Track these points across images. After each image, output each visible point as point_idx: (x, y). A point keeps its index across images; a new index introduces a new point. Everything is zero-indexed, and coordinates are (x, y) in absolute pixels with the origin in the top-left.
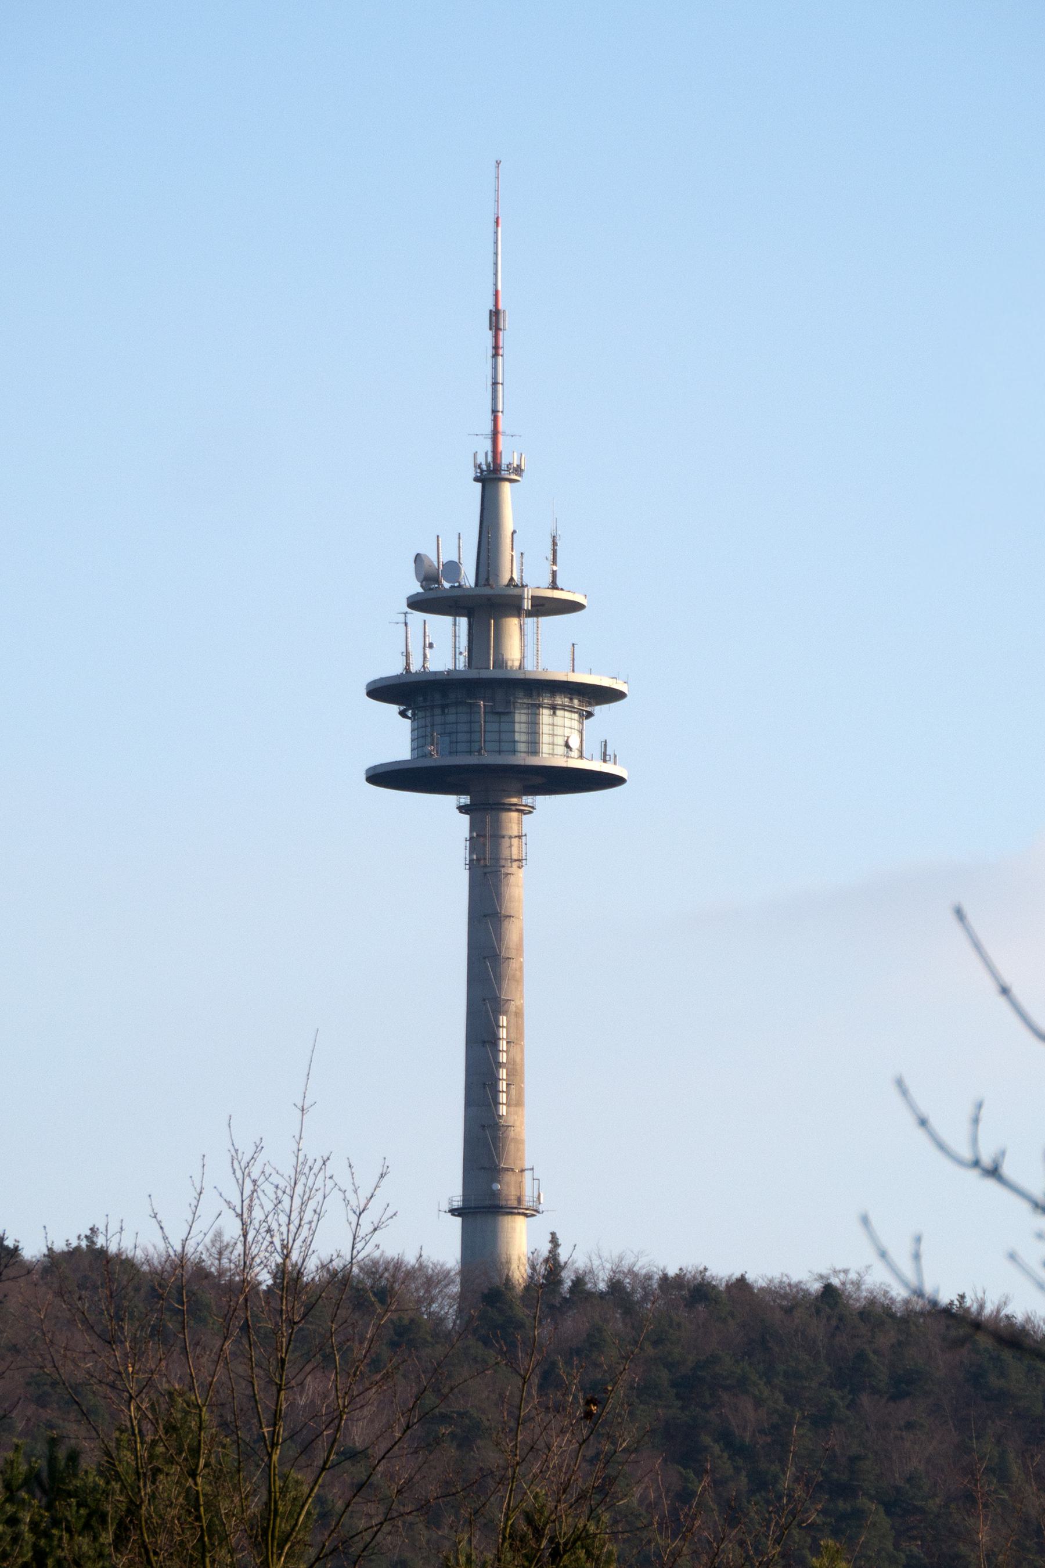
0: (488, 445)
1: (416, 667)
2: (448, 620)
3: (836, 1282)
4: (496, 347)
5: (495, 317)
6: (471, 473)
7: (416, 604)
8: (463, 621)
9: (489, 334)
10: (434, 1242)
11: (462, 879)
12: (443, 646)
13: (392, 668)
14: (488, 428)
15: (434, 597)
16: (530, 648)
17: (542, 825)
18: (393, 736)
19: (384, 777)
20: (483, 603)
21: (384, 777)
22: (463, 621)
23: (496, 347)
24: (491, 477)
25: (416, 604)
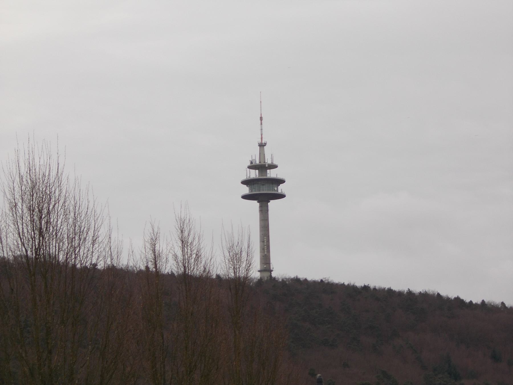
0: (260, 140)
1: (242, 273)
2: (254, 170)
3: (324, 280)
4: (261, 123)
5: (261, 119)
6: (258, 145)
7: (250, 167)
8: (257, 171)
9: (260, 121)
10: (255, 274)
11: (272, 261)
12: (254, 174)
13: (244, 178)
14: (260, 137)
15: (252, 167)
16: (272, 174)
17: (273, 204)
18: (246, 190)
19: (245, 197)
20: (262, 167)
21: (245, 197)
22: (257, 171)
23: (261, 123)
24: (262, 145)
25: (250, 167)
